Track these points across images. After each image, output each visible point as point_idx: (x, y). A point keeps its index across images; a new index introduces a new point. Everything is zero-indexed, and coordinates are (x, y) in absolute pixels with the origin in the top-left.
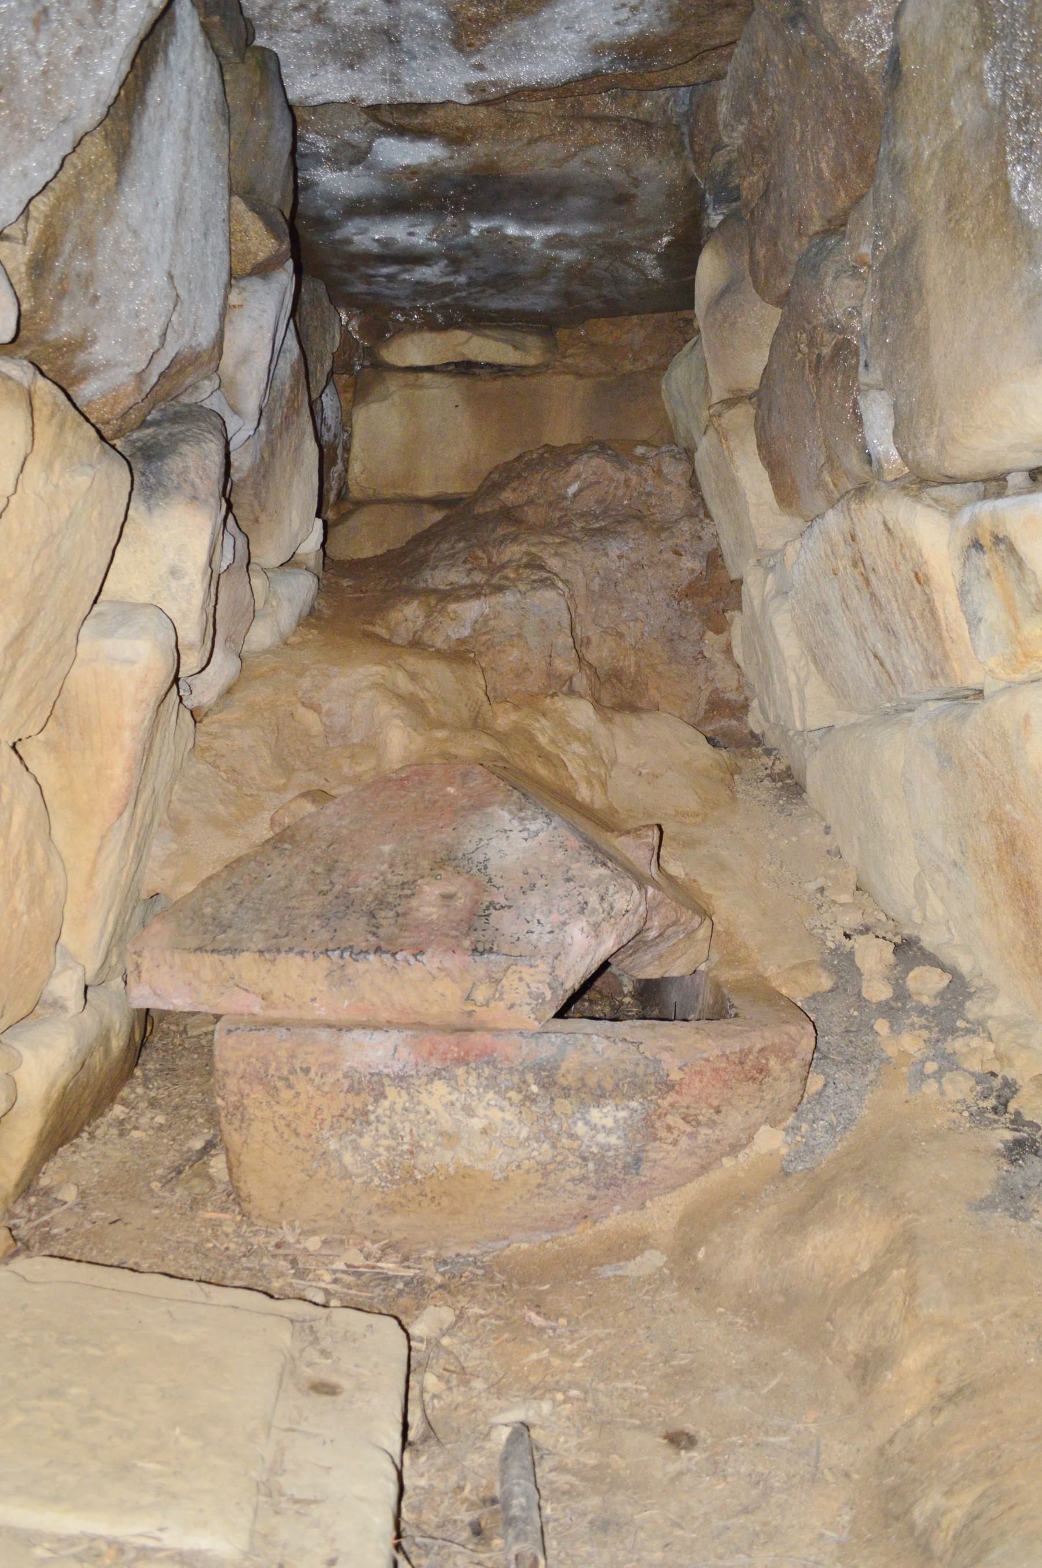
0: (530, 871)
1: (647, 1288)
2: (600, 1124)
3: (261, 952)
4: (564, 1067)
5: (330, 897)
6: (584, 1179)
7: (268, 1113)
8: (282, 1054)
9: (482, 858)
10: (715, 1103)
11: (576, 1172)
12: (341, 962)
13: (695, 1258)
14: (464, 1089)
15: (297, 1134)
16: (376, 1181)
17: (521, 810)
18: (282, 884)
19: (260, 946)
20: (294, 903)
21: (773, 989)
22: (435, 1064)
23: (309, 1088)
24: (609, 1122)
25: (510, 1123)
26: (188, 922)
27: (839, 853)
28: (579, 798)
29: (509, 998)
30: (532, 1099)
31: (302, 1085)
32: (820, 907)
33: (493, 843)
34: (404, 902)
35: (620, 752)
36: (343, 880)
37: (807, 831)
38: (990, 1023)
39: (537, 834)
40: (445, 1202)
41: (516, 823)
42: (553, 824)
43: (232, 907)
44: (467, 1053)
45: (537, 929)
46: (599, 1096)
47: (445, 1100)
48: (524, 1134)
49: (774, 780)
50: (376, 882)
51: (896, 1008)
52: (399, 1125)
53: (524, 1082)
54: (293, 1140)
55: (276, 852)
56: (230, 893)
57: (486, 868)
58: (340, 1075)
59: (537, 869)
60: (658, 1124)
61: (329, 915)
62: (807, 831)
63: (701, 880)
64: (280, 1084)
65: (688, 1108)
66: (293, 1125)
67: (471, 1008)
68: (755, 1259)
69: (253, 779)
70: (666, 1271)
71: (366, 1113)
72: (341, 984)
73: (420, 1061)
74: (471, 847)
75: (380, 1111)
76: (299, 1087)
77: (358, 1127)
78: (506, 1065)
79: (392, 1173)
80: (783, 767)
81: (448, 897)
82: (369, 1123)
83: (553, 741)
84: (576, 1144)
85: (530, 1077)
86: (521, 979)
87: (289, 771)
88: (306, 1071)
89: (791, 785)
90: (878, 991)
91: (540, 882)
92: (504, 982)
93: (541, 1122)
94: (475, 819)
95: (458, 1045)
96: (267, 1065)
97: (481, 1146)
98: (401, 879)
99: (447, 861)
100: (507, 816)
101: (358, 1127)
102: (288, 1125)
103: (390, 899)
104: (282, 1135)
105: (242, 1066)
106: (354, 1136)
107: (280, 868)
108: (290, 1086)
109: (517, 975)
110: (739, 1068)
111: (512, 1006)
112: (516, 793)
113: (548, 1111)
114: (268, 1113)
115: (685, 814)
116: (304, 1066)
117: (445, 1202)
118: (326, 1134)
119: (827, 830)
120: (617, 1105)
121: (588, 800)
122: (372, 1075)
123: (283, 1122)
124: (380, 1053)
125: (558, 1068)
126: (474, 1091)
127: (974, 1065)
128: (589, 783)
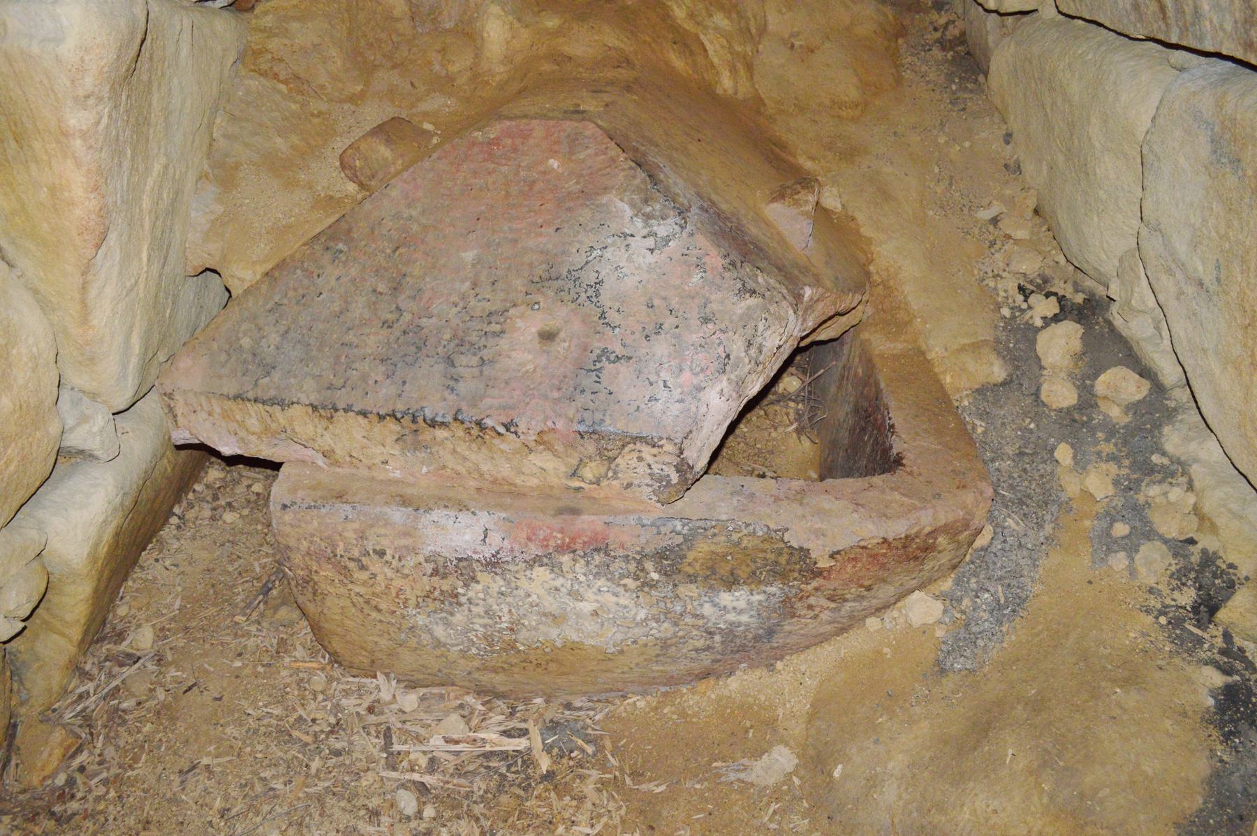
0: (656, 302)
1: (774, 807)
2: (730, 606)
3: (315, 408)
4: (691, 556)
5: (397, 331)
6: (708, 648)
7: (342, 590)
8: (350, 535)
9: (592, 278)
10: (867, 583)
11: (700, 644)
12: (414, 427)
13: (830, 775)
14: (570, 576)
15: (379, 611)
16: (474, 651)
17: (646, 201)
18: (336, 307)
19: (314, 398)
20: (351, 337)
21: (936, 374)
22: (534, 550)
23: (386, 570)
24: (742, 604)
25: (625, 607)
26: (223, 357)
27: (1018, 169)
28: (719, 91)
29: (625, 477)
30: (653, 585)
31: (376, 565)
32: (992, 244)
33: (608, 254)
34: (491, 342)
35: (770, 19)
36: (413, 306)
37: (983, 135)
38: (1195, 470)
39: (667, 240)
40: (553, 667)
41: (639, 223)
42: (689, 228)
43: (274, 338)
44: (573, 540)
45: (663, 394)
46: (731, 583)
47: (547, 586)
48: (642, 615)
49: (943, 49)
50: (455, 310)
51: (1079, 421)
52: (495, 607)
53: (643, 570)
54: (374, 614)
55: (328, 256)
56: (271, 318)
57: (597, 295)
58: (421, 559)
59: (665, 299)
60: (798, 605)
61: (395, 359)
62: (983, 135)
63: (860, 217)
64: (351, 565)
65: (835, 590)
66: (373, 603)
67: (577, 484)
68: (900, 798)
69: (322, 87)
70: (796, 781)
71: (456, 596)
72: (415, 449)
73: (516, 547)
74: (580, 260)
75: (471, 594)
76: (373, 569)
77: (447, 607)
78: (621, 552)
79: (491, 645)
80: (957, 32)
81: (548, 336)
82: (460, 605)
83: (691, 16)
84: (701, 622)
85: (649, 565)
86: (640, 459)
87: (367, 70)
88: (382, 554)
89: (968, 62)
90: (1060, 394)
91: (669, 322)
92: (619, 460)
93: (662, 604)
94: (585, 215)
95: (562, 531)
96: (334, 546)
97: (590, 626)
98: (488, 307)
99: (552, 279)
100: (628, 211)
101: (447, 607)
102: (368, 602)
103: (474, 338)
104: (362, 610)
105: (305, 544)
106: (444, 615)
107: (333, 282)
108: (363, 568)
109: (635, 455)
110: (902, 551)
111: (629, 485)
112: (641, 175)
113: (670, 594)
114: (342, 590)
115: (841, 105)
116: (378, 548)
117: (553, 667)
118: (411, 611)
119: (1008, 138)
120: (752, 590)
121: (730, 92)
122: (460, 560)
123: (361, 600)
124: (467, 537)
125: (684, 557)
126: (582, 578)
127: (1171, 527)
128: (733, 70)
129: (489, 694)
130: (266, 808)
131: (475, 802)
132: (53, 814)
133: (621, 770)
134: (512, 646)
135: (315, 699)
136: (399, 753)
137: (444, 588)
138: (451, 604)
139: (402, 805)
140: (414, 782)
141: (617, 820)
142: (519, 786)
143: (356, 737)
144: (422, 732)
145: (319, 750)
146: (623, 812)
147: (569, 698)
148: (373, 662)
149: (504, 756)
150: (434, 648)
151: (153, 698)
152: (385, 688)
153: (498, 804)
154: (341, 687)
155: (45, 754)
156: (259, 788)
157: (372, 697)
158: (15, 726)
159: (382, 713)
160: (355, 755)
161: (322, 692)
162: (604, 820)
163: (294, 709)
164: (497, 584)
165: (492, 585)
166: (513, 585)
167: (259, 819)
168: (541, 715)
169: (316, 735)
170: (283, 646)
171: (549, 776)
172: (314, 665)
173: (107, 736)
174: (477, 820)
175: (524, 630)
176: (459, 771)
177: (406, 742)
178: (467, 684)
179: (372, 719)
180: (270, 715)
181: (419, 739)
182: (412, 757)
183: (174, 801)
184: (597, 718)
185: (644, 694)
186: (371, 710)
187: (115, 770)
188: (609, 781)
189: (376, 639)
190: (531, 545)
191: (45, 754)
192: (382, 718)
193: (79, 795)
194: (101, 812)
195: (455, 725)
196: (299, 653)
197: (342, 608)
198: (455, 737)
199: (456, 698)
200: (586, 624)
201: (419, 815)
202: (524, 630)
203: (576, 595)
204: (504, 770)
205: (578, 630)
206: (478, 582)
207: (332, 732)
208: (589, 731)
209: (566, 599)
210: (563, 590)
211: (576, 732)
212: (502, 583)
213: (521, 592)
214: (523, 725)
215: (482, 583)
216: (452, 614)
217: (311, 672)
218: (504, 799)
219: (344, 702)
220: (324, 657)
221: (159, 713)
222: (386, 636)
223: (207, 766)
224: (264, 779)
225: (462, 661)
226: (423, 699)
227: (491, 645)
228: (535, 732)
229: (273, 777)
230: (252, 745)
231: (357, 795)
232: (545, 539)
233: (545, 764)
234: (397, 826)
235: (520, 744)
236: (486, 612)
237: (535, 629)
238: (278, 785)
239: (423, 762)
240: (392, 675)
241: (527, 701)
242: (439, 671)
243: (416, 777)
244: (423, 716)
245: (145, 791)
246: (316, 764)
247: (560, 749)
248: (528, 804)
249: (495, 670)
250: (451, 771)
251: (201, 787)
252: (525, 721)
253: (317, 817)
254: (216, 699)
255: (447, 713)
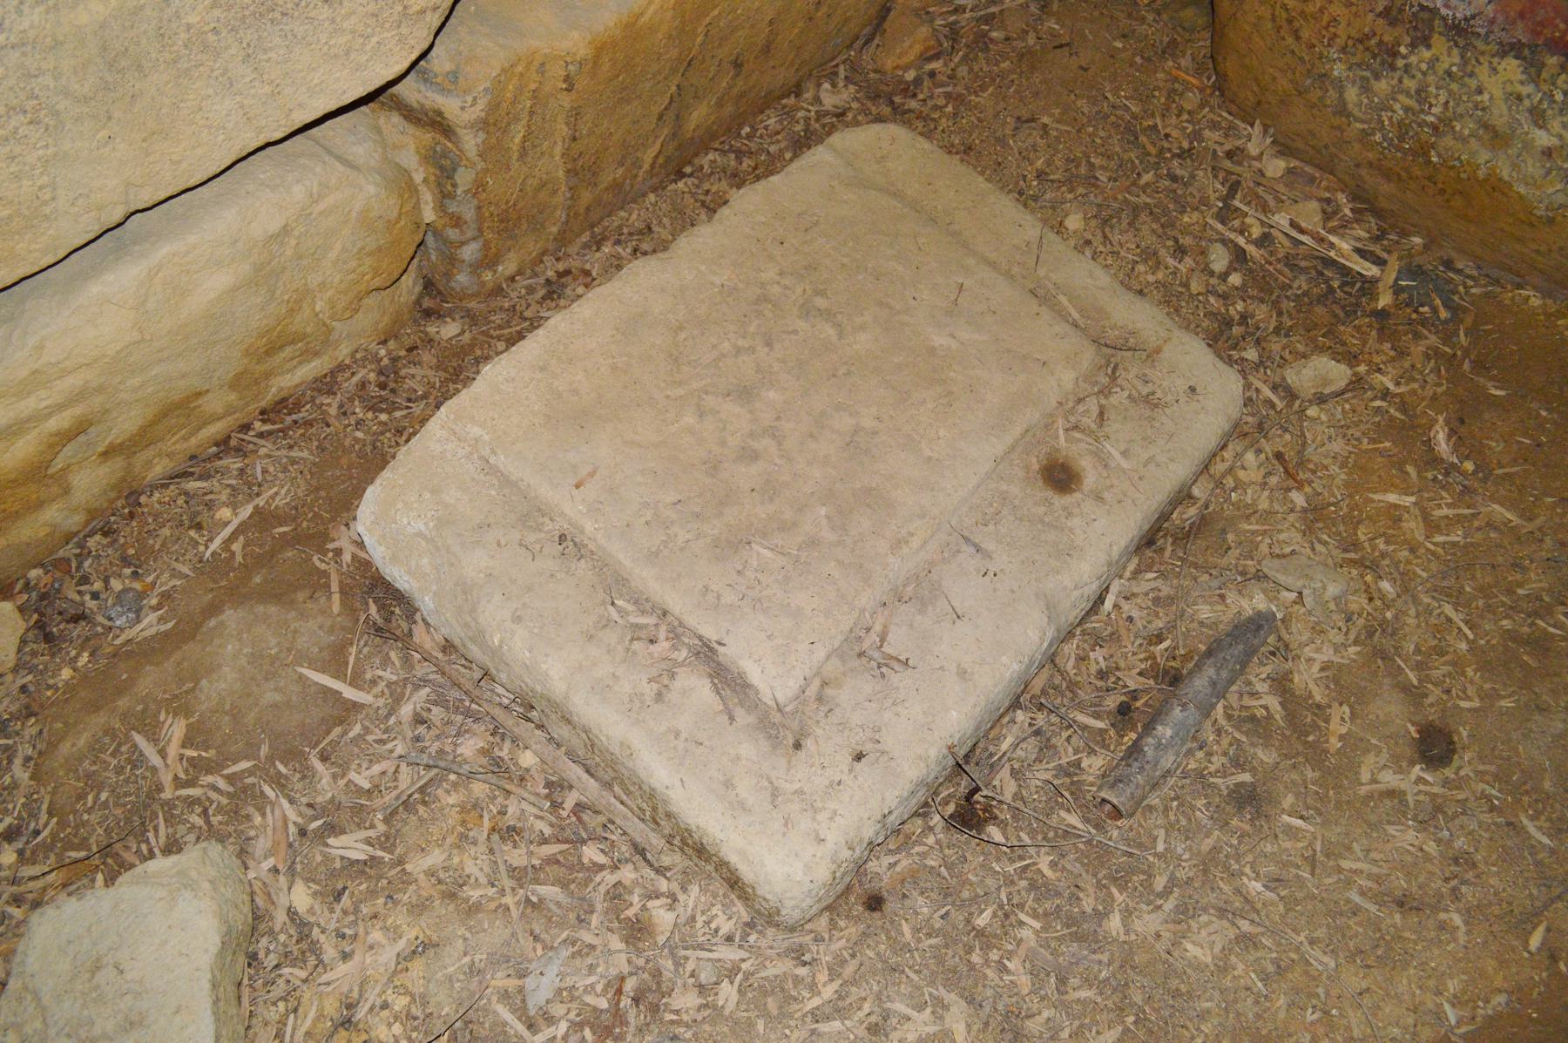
14: (1545, 88)
15: (1298, 38)
16: (1378, 137)
22: (1521, 33)
47: (1509, 89)
52: (1432, 89)
54: (1290, 40)
66: (1296, 24)
73: (1500, 19)
75: (1413, 59)
77: (1376, 65)
79: (1401, 139)
82: (1393, 68)
97: (1533, 167)
101: (1376, 65)
102: (1290, 21)
106: (1367, 74)
117: (1458, 202)
123: (1284, 15)
129: (1366, 204)
130: (1081, 190)
131: (1288, 298)
132: (892, 102)
133: (1466, 353)
134: (1423, 150)
135: (1178, 116)
136: (1237, 209)
137: (1386, 38)
138: (1382, 64)
139: (1213, 257)
140: (1236, 245)
141: (1429, 392)
142: (1343, 308)
143: (1201, 173)
144: (1272, 203)
145: (1157, 166)
146: (1440, 390)
147: (1454, 255)
148: (1259, 103)
149: (1345, 271)
150: (1335, 114)
151: (1024, 40)
152: (1256, 141)
153: (1309, 311)
154: (1211, 116)
155: (907, 44)
156: (1083, 170)
157: (1238, 143)
158: (889, 10)
159: (1240, 164)
160: (1190, 189)
161: (1189, 113)
162: (1415, 386)
163: (1153, 115)
164: (1450, 60)
165: (1444, 58)
166: (1469, 69)
167: (1070, 196)
168: (1410, 256)
169: (1161, 151)
170: (1172, 49)
171: (1382, 314)
172: (1194, 81)
173: (965, 57)
174: (1280, 314)
175: (1450, 137)
176: (1289, 262)
177: (1248, 204)
178: (1347, 178)
179: (1228, 164)
180: (1127, 109)
181: (1265, 209)
182: (1248, 220)
183: (1002, 141)
184: (1473, 291)
185: (1546, 294)
186: (1229, 155)
187: (960, 89)
188: (1444, 354)
189: (1277, 74)
190: (1520, 25)
191: (907, 44)
192: (1238, 169)
193: (921, 97)
194: (933, 120)
195: (1310, 215)
196: (1185, 62)
197: (1259, 18)
198: (1303, 225)
199: (1327, 189)
200: (1530, 162)
201: (1224, 276)
202: (1450, 137)
203: (1538, 117)
204: (1336, 284)
205: (1515, 166)
206: (1429, 47)
207: (1179, 156)
208: (1456, 298)
209: (1523, 117)
210: (1527, 103)
211: (1437, 290)
212: (1457, 60)
213: (1473, 83)
214: (1385, 255)
215: (1434, 51)
216: (1377, 77)
217: (1188, 87)
218: (1320, 310)
219: (1207, 133)
220: (1209, 78)
221: (1022, 55)
222: (1289, 74)
223: (1045, 126)
224: (1091, 165)
225: (1357, 146)
226: (1290, 171)
227: (1401, 139)
228: (1394, 265)
229: (1102, 167)
230: (1096, 129)
231: (1173, 226)
232: (1541, 24)
233: (1385, 300)
234: (1197, 273)
235: (1371, 270)
236: (1418, 92)
237: (1465, 140)
238: (1103, 177)
239: (1256, 232)
240: (1272, 131)
241: (1404, 234)
242: (1326, 147)
243: (1241, 241)
244: (1281, 188)
245: (980, 120)
246: (1147, 177)
247: (1411, 297)
248: (1342, 328)
249: (1388, 175)
250: (1280, 256)
251: (1030, 141)
252: (1389, 252)
253: (1124, 224)
254: (1081, 68)
255: (1308, 197)
